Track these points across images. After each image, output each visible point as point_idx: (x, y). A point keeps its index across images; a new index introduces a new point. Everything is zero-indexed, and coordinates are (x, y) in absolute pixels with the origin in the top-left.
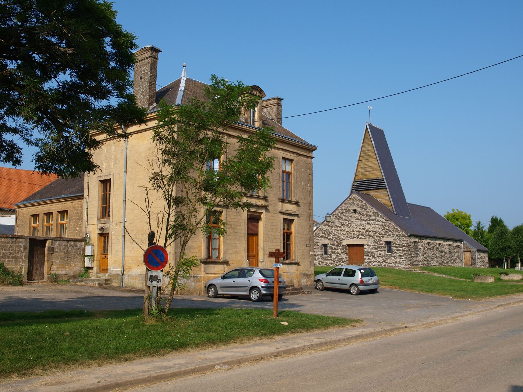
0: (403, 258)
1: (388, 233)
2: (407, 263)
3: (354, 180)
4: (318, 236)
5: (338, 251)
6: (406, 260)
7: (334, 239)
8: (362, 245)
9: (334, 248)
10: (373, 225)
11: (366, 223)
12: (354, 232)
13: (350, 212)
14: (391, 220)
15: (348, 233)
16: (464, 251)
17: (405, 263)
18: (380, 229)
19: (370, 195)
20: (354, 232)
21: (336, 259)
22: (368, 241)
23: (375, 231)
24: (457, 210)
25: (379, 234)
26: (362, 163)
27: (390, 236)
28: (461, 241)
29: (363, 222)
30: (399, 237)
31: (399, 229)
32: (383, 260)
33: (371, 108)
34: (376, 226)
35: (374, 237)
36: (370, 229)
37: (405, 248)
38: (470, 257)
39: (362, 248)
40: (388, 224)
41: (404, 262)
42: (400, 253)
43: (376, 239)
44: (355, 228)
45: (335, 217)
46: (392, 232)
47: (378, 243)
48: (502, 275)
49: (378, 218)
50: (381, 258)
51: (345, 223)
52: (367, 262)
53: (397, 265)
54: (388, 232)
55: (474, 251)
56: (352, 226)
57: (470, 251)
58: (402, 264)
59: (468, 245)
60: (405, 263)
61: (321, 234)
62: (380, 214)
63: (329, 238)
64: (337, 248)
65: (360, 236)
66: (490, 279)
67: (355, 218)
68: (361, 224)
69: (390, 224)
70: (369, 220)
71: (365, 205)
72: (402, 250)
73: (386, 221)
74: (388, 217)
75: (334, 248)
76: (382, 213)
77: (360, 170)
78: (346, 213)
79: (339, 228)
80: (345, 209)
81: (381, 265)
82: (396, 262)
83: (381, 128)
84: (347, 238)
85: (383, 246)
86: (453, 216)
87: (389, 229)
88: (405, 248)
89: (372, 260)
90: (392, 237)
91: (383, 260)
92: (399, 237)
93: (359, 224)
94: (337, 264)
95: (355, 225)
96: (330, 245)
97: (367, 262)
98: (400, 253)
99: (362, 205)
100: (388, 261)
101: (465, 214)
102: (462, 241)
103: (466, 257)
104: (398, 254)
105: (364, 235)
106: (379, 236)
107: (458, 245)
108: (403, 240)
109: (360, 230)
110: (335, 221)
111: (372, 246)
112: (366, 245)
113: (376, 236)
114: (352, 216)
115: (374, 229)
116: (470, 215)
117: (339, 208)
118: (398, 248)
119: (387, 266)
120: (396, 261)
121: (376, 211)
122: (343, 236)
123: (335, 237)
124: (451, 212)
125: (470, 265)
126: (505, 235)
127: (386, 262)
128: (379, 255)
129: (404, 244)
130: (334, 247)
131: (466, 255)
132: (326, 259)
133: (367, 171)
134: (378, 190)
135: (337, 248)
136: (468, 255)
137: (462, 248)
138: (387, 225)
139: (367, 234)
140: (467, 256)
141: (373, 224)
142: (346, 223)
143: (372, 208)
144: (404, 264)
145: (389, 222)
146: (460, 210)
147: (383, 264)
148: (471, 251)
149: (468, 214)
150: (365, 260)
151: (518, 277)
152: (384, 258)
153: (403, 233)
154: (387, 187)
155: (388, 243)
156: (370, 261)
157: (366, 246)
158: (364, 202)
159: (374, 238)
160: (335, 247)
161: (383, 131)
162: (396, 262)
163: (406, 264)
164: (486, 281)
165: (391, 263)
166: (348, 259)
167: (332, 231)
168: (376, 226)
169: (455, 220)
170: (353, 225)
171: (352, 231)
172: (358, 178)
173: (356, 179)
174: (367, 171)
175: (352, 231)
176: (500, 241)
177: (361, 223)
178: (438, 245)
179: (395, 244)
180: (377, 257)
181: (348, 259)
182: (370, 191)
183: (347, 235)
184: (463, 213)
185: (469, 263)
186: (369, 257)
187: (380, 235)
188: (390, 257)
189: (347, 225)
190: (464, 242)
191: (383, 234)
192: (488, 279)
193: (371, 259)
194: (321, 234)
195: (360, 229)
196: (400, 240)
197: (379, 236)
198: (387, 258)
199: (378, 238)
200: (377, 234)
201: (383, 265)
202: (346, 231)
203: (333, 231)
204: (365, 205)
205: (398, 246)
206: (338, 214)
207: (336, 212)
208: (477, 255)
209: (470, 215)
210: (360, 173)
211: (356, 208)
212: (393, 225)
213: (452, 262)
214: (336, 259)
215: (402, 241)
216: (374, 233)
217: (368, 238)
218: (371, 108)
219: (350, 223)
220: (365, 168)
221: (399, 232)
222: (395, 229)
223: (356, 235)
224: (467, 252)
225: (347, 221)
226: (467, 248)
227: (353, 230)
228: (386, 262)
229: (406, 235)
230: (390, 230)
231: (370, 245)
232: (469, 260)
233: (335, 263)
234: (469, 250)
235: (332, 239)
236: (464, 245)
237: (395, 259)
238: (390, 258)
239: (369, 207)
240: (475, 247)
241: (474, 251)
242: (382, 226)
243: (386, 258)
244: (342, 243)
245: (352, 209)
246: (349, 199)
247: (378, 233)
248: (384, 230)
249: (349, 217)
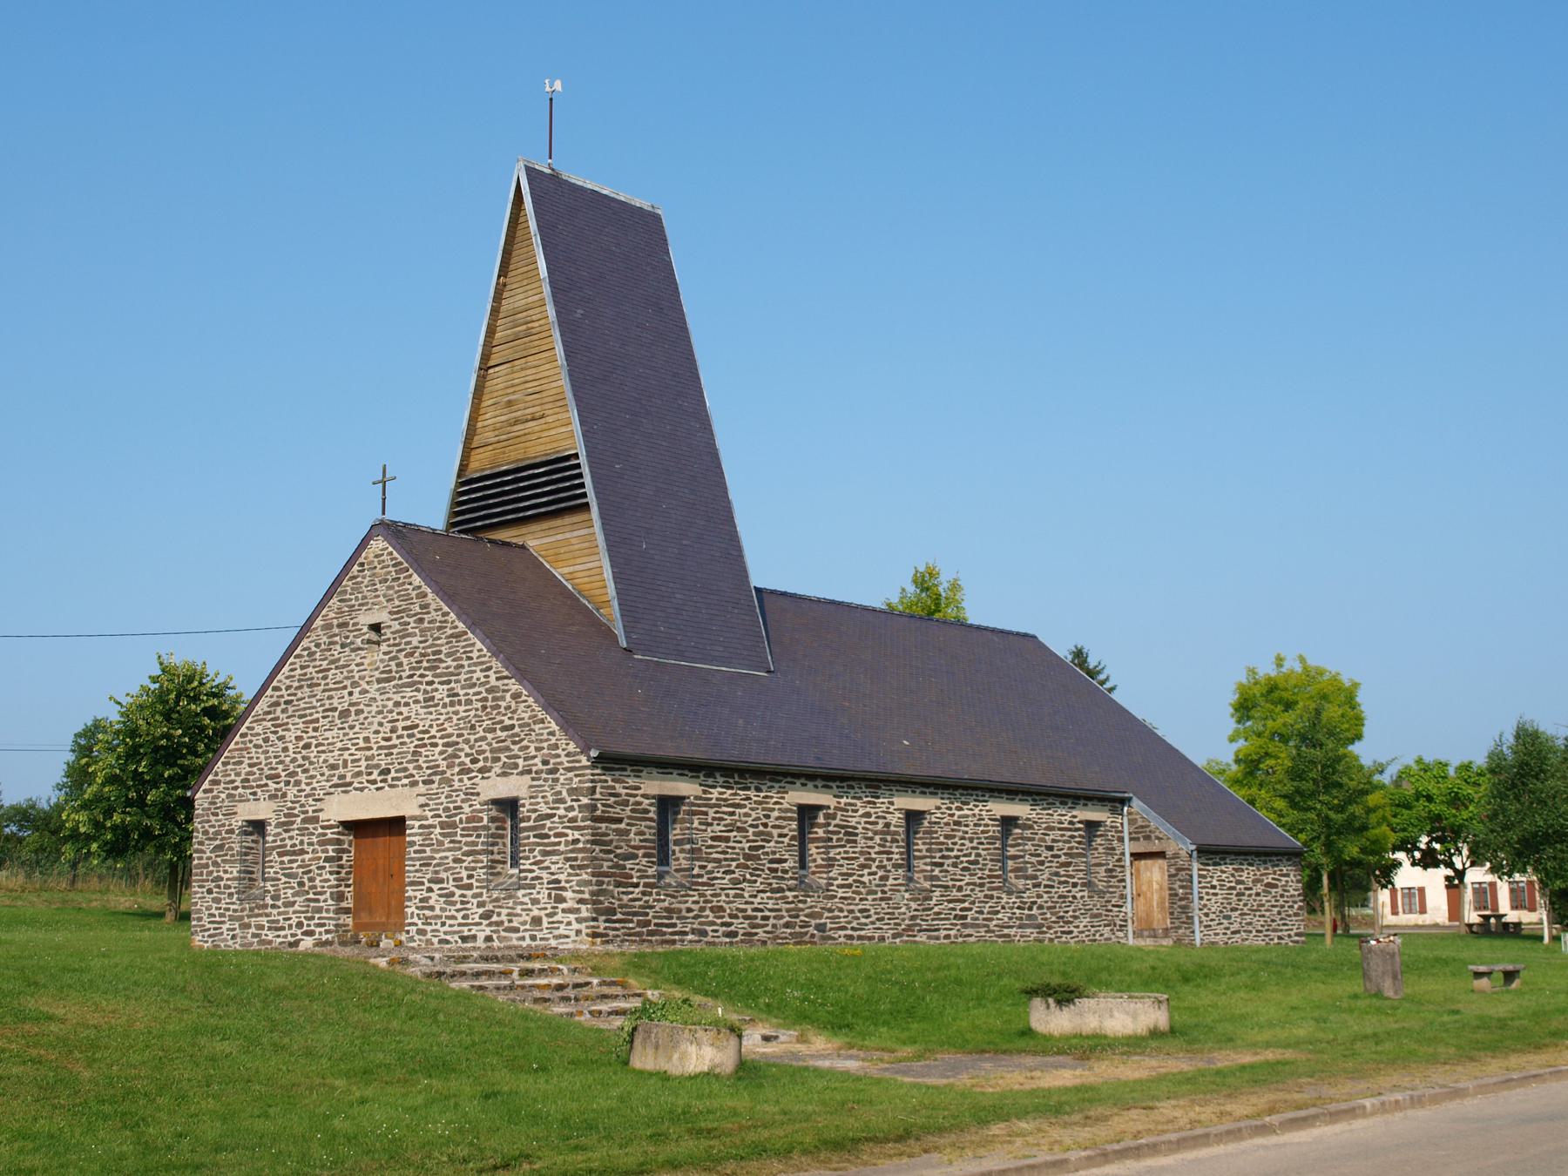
0: (568, 894)
1: (508, 749)
2: (582, 926)
3: (459, 476)
4: (233, 777)
5: (307, 857)
6: (578, 911)
7: (290, 796)
8: (395, 826)
9: (289, 842)
10: (445, 706)
11: (420, 697)
12: (369, 753)
13: (359, 641)
14: (521, 674)
15: (346, 755)
16: (1137, 856)
17: (575, 926)
18: (473, 727)
19: (523, 547)
20: (369, 753)
21: (297, 907)
22: (423, 800)
23: (454, 738)
24: (1302, 659)
25: (467, 760)
26: (499, 378)
27: (516, 766)
28: (1117, 803)
29: (408, 692)
30: (554, 771)
31: (554, 727)
32: (481, 911)
33: (558, 86)
34: (456, 713)
35: (448, 774)
36: (433, 732)
37: (577, 835)
38: (1166, 885)
39: (394, 839)
40: (508, 697)
41: (572, 917)
42: (556, 864)
43: (456, 785)
44: (375, 727)
45: (299, 671)
46: (525, 743)
47: (467, 809)
48: (1037, 1002)
49: (466, 663)
50: (475, 896)
51: (335, 702)
52: (415, 920)
53: (539, 935)
54: (508, 743)
55: (1183, 853)
56: (362, 716)
57: (1160, 855)
58: (562, 930)
59: (1156, 822)
60: (575, 926)
61: (245, 768)
62: (479, 645)
63: (272, 786)
64: (302, 843)
65: (393, 774)
66: (693, 1049)
67: (377, 674)
68: (397, 704)
69: (516, 696)
70: (429, 678)
71: (418, 596)
72: (562, 848)
73: (499, 683)
74: (508, 662)
75: (289, 842)
76: (489, 637)
77: (489, 418)
78: (343, 646)
79: (312, 734)
80: (339, 626)
81: (474, 937)
82: (537, 921)
83: (646, 205)
84: (344, 785)
85: (486, 828)
86: (1272, 688)
87: (512, 727)
88: (577, 835)
89: (438, 912)
90: (522, 773)
91: (481, 911)
92: (554, 771)
93: (390, 704)
94: (299, 932)
95: (374, 709)
96: (277, 826)
97: (415, 920)
98: (554, 868)
99: (408, 598)
100: (504, 911)
101: (1335, 679)
102: (1123, 801)
103: (1144, 888)
104: (544, 874)
105: (411, 766)
106: (469, 771)
107: (1092, 826)
108: (571, 791)
109: (395, 741)
110: (300, 695)
111: (438, 830)
112: (417, 824)
113: (457, 769)
114: (366, 661)
115: (450, 730)
116: (1356, 685)
117: (319, 622)
118: (547, 836)
119: (496, 944)
120: (536, 913)
121: (461, 626)
122: (327, 773)
123: (298, 783)
124: (1267, 669)
125: (1166, 930)
126: (1536, 777)
127: (495, 918)
128: (466, 881)
129: (571, 815)
130: (291, 838)
131: (1145, 876)
132: (258, 907)
133: (517, 422)
134: (558, 522)
135: (302, 843)
136: (1155, 873)
137: (1121, 840)
138: (503, 704)
139: (422, 760)
140: (1150, 883)
141: (447, 700)
142: (340, 701)
143: (446, 609)
144: (572, 934)
145: (514, 686)
146: (1313, 662)
147: (482, 932)
148: (1169, 853)
149: (1346, 680)
150: (409, 911)
151: (1134, 1016)
152: (484, 898)
153: (572, 747)
154: (592, 498)
155: (509, 806)
156: (428, 913)
157: (413, 833)
158: (416, 580)
159: (449, 782)
160: (293, 839)
161: (657, 219)
162: (537, 921)
163: (578, 932)
164: (675, 1066)
165: (515, 924)
166: (348, 903)
167: (285, 749)
168: (456, 713)
169: (1280, 708)
170: (366, 709)
171: (362, 744)
172: (481, 463)
173: (474, 465)
174: (517, 422)
175: (362, 744)
176: (1513, 807)
177: (397, 698)
178: (896, 819)
179: (534, 816)
180: (458, 892)
181: (348, 903)
182: (524, 530)
183: (341, 771)
184: (1326, 677)
185: (1161, 920)
186: (426, 894)
187: (475, 761)
188: (510, 892)
189: (344, 714)
190: (1137, 804)
191: (486, 759)
192: (683, 1047)
193: (432, 902)
194: (245, 768)
195: (393, 730)
196: (558, 788)
197: (469, 771)
198: (497, 900)
199: (465, 777)
200: (463, 759)
201: (481, 936)
202: (339, 745)
203: (291, 746)
204: (418, 596)
205: (548, 823)
206: (311, 654)
207: (305, 643)
208: (1195, 873)
209: (1356, 685)
210: (489, 436)
211: (381, 616)
212: (531, 700)
213: (1030, 917)
214: (297, 907)
215: (564, 794)
216: (450, 750)
217: (424, 782)
218: (558, 86)
219: (354, 698)
220: (510, 403)
221: (553, 741)
222: (537, 727)
223: (377, 766)
224: (1149, 862)
225: (345, 692)
226: (1147, 838)
227: (367, 740)
228: (495, 918)
229: (584, 759)
230: (517, 730)
231: (430, 821)
232: (1161, 903)
233: (290, 926)
234: (1155, 847)
235: (284, 795)
236: (1131, 822)
237: (535, 902)
238: (510, 897)
239: (433, 606)
240: (1185, 829)
241: (1183, 853)
242: (484, 708)
243: (495, 894)
244: (322, 816)
245: (366, 619)
246: (356, 568)
247: (468, 750)
248: (490, 736)
249: (353, 667)
